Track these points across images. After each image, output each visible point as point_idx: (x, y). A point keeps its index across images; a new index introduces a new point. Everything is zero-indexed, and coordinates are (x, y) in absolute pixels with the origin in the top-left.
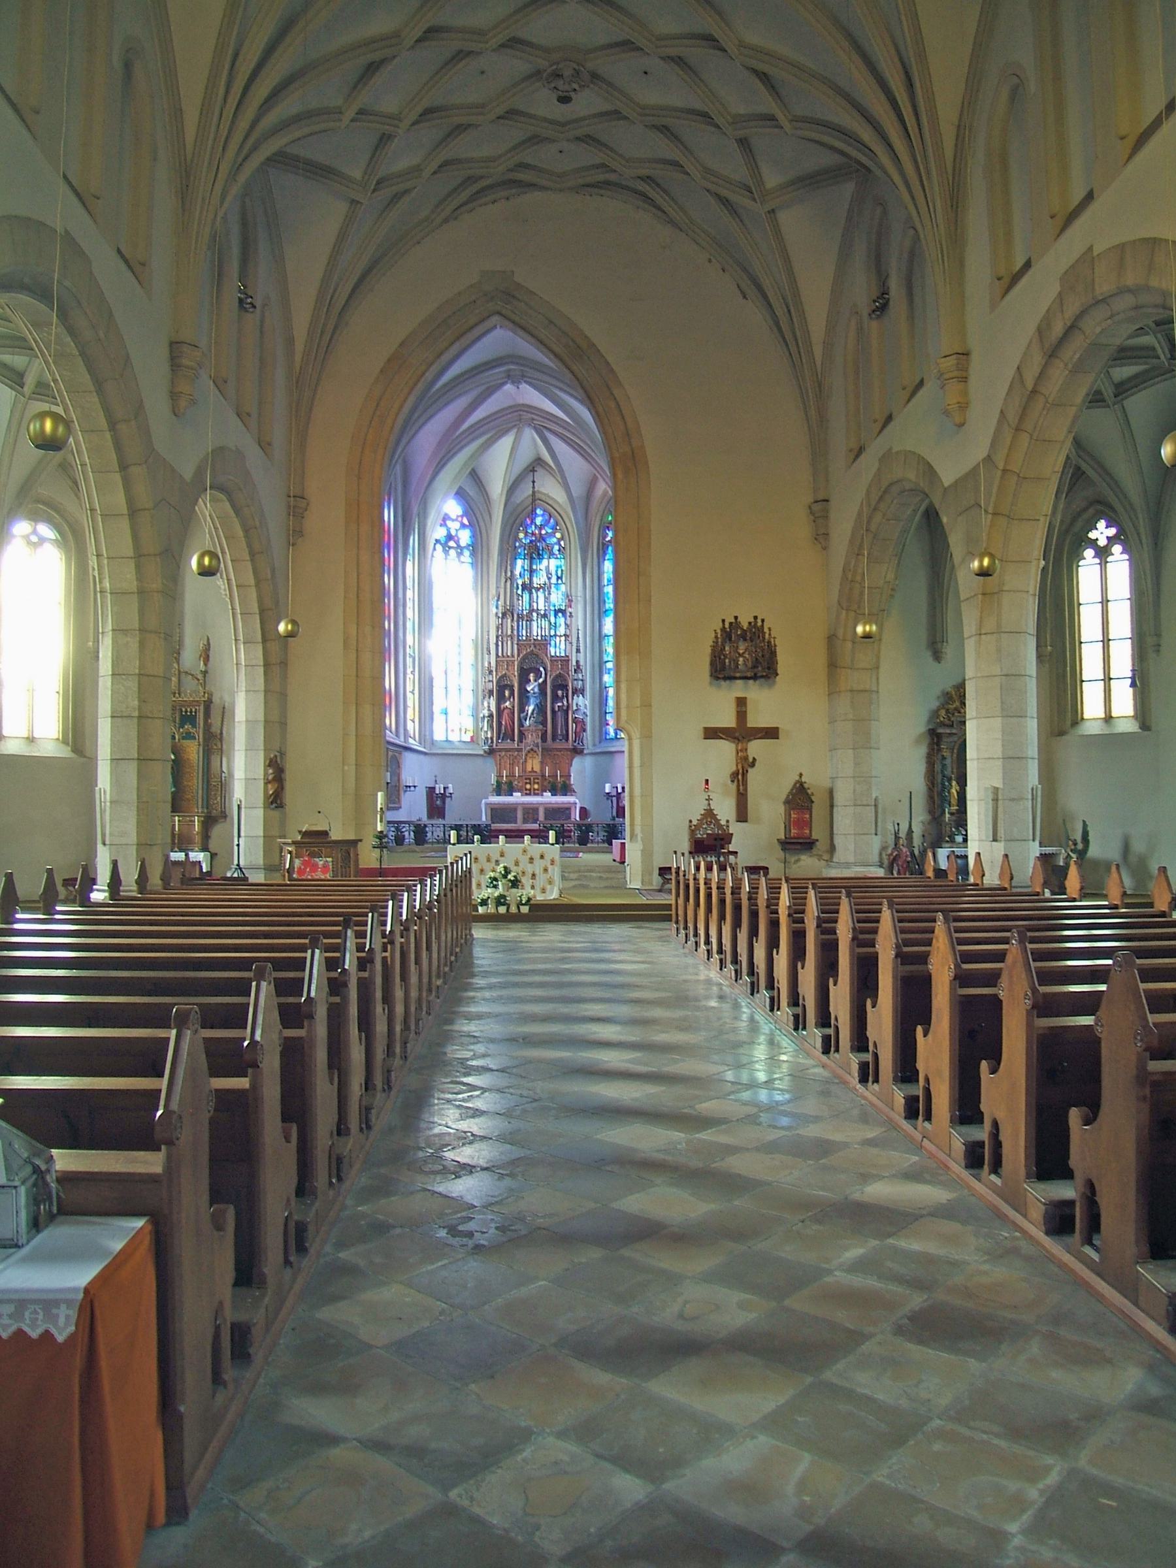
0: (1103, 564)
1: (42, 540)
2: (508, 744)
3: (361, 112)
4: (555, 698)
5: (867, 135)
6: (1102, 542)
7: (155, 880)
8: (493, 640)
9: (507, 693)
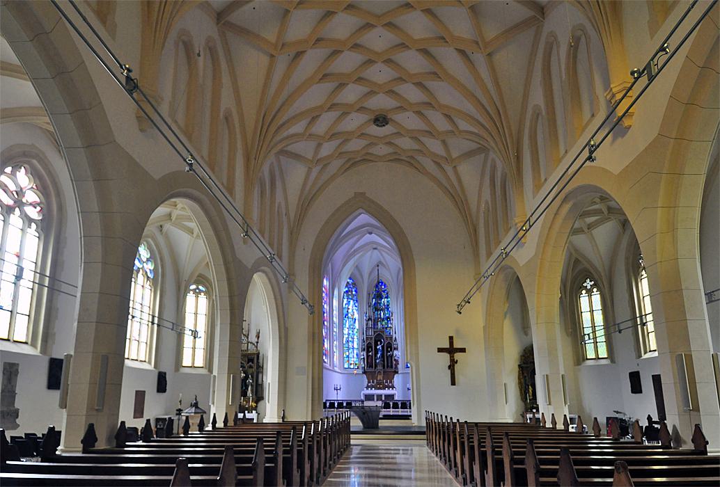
0: (590, 296)
1: (201, 291)
3: (310, 135)
5: (486, 135)
6: (589, 287)
7: (231, 423)
8: (365, 329)
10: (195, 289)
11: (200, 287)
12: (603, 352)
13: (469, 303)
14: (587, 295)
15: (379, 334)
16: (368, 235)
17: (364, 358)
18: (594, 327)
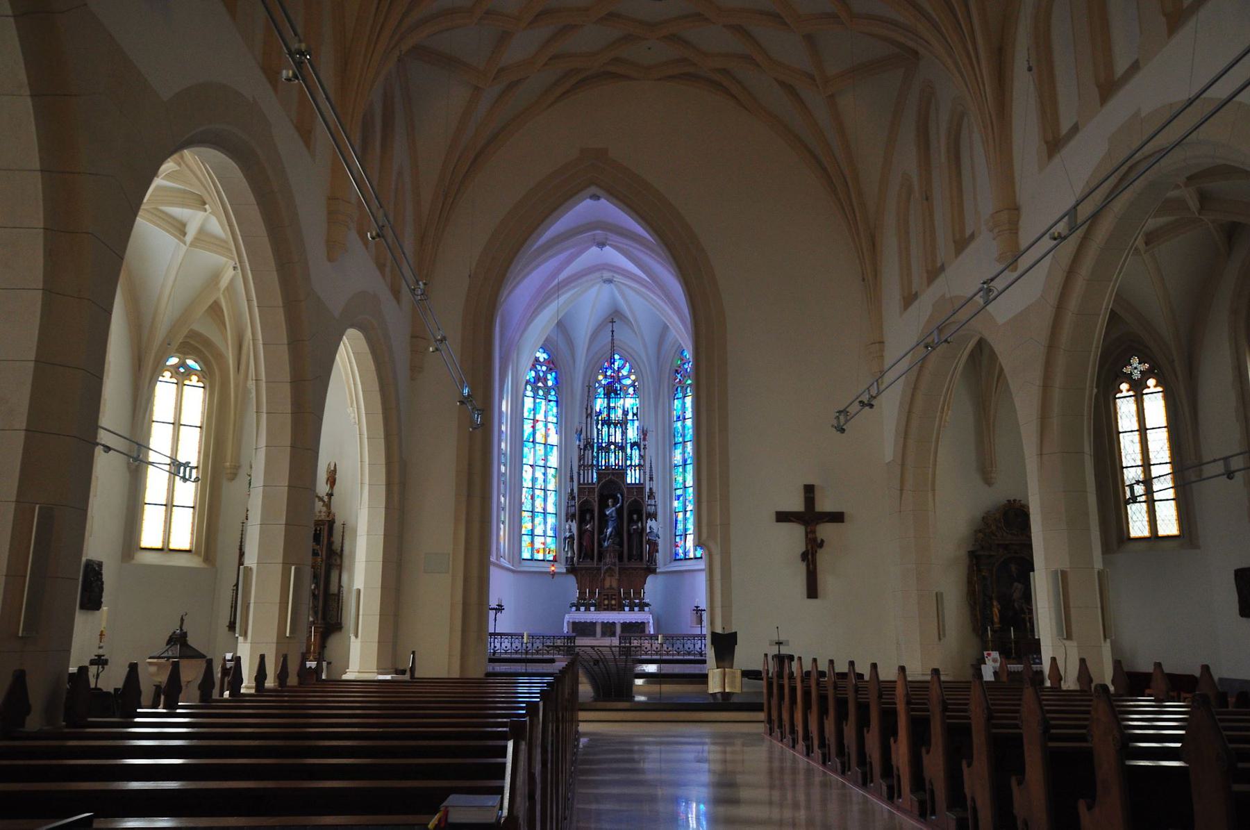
1: (189, 372)
2: (588, 564)
4: (631, 521)
6: (1137, 375)
7: (293, 680)
9: (588, 517)
10: (177, 367)
11: (190, 362)
12: (1168, 524)
13: (871, 406)
14: (1131, 393)
15: (611, 481)
16: (595, 249)
17: (571, 537)
18: (1146, 464)
